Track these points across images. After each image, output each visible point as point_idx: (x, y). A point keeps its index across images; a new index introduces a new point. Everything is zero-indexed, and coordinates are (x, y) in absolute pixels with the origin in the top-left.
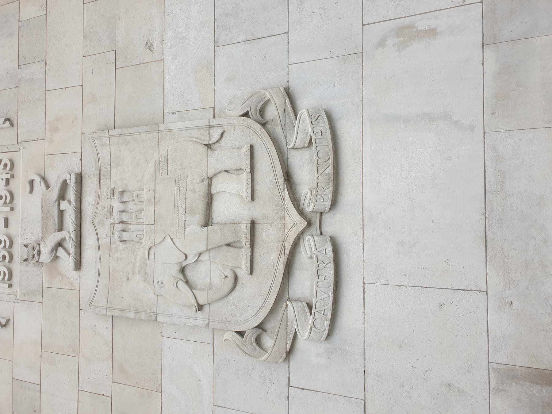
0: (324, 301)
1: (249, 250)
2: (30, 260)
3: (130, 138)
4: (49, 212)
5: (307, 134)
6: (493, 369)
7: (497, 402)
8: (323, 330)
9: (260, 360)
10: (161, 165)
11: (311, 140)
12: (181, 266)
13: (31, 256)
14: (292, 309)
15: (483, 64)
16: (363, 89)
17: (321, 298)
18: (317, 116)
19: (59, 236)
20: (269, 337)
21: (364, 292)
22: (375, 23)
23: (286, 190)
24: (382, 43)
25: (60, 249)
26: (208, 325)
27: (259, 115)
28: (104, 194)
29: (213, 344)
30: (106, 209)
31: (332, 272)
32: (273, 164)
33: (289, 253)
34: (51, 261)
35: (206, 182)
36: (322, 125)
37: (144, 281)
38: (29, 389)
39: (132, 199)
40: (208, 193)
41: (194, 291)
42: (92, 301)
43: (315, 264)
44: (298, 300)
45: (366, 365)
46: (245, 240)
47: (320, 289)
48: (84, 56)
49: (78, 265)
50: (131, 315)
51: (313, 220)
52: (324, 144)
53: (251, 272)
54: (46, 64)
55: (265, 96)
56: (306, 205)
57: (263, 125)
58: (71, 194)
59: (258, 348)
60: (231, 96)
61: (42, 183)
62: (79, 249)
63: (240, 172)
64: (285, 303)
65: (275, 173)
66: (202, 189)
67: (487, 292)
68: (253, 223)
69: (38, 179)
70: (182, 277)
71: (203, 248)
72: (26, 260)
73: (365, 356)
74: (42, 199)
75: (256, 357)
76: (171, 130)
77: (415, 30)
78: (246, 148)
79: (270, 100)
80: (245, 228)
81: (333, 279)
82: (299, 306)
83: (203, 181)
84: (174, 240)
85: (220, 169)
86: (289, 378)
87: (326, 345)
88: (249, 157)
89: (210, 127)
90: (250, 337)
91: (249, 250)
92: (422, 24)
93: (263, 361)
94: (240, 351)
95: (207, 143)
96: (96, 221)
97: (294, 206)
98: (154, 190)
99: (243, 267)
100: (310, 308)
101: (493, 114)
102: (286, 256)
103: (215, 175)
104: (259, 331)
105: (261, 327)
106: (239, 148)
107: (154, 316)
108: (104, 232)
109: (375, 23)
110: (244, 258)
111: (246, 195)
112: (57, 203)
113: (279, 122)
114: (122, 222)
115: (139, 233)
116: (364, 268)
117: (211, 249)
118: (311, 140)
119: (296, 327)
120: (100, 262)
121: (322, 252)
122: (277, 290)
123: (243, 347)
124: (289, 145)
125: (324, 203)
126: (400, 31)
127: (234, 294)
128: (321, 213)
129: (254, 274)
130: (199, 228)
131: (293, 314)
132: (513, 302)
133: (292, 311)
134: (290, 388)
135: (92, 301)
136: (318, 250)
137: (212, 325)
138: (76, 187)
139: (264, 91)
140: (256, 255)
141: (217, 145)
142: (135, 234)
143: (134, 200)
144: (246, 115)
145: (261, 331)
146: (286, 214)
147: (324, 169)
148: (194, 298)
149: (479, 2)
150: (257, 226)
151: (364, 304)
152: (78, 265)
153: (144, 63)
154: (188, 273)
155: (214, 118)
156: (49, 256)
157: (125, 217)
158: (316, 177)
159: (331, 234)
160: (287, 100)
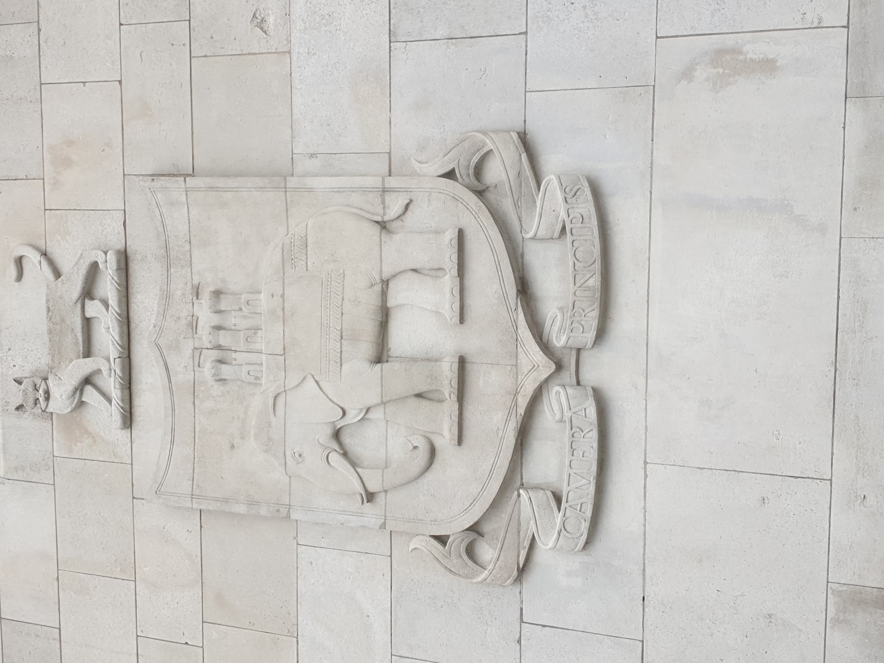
0: (580, 491)
1: (456, 406)
2: (28, 408)
3: (229, 195)
4: (63, 320)
5: (558, 217)
6: (833, 591)
7: (836, 637)
8: (578, 535)
9: (475, 581)
10: (294, 252)
11: (564, 228)
12: (335, 427)
13: (31, 401)
14: (528, 503)
15: (844, 128)
16: (652, 149)
17: (576, 485)
18: (574, 190)
19: (86, 366)
20: (489, 545)
21: (646, 476)
22: (677, 36)
23: (520, 310)
24: (687, 74)
25: (89, 389)
26: (383, 526)
27: (472, 177)
28: (179, 293)
29: (391, 556)
30: (184, 322)
31: (595, 445)
32: (498, 265)
33: (525, 413)
34: (73, 411)
35: (378, 288)
36: (584, 205)
37: (266, 451)
38: (37, 636)
39: (237, 308)
40: (382, 306)
41: (359, 470)
42: (161, 484)
43: (568, 432)
44: (537, 488)
45: (646, 588)
46: (448, 390)
47: (575, 471)
48: (121, 24)
49: (128, 419)
50: (241, 509)
51: (565, 360)
52: (586, 238)
53: (460, 441)
54: (39, 30)
55: (484, 144)
56: (554, 336)
57: (480, 193)
58: (108, 286)
59: (470, 563)
60: (425, 135)
61: (45, 264)
62: (127, 391)
63: (439, 273)
64: (516, 493)
65: (501, 280)
66: (371, 299)
67: (831, 480)
68: (462, 362)
69: (33, 258)
70: (336, 447)
71: (373, 398)
72: (19, 408)
73: (644, 575)
74: (47, 295)
75: (466, 577)
76: (311, 190)
77: (741, 57)
78: (450, 235)
79: (490, 151)
80: (448, 370)
81: (596, 457)
82: (540, 497)
83: (372, 285)
84: (321, 383)
85: (403, 267)
86: (522, 609)
87: (584, 558)
88: (456, 250)
89: (384, 191)
90: (457, 544)
91: (456, 406)
92: (755, 49)
93: (480, 582)
94: (438, 566)
95: (379, 219)
96: (162, 342)
97: (534, 337)
98: (283, 296)
99: (446, 433)
100: (558, 499)
101: (855, 209)
102: (520, 419)
103: (394, 276)
104: (472, 536)
105: (475, 529)
106: (438, 232)
107: (283, 511)
108: (180, 362)
109: (677, 36)
110: (447, 418)
111: (449, 309)
112: (79, 305)
113: (509, 193)
114: (219, 347)
115: (252, 368)
116: (646, 440)
117: (389, 401)
118: (564, 228)
119: (534, 530)
120: (173, 415)
121: (579, 413)
122: (504, 471)
123: (445, 562)
124: (526, 233)
125: (585, 335)
126: (718, 56)
127: (430, 476)
128: (579, 350)
129: (464, 445)
130: (366, 365)
131: (529, 509)
132: (867, 496)
133: (527, 504)
134: (523, 625)
135: (161, 484)
136: (573, 410)
137: (390, 526)
138: (119, 278)
139: (483, 137)
140: (467, 414)
141: (398, 223)
142: (245, 369)
143: (241, 309)
144: (450, 175)
145: (476, 535)
146: (520, 349)
147: (585, 279)
148: (359, 481)
149: (843, 27)
150: (469, 367)
151: (645, 496)
152: (128, 419)
153: (249, 54)
154: (346, 439)
155: (390, 175)
156: (67, 402)
157: (224, 339)
158: (572, 291)
159: (595, 384)
160: (524, 156)
